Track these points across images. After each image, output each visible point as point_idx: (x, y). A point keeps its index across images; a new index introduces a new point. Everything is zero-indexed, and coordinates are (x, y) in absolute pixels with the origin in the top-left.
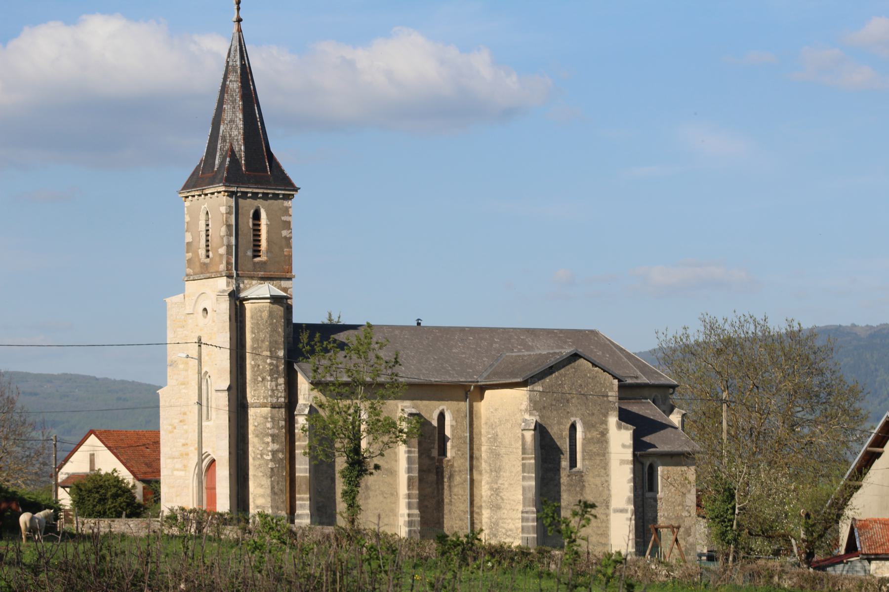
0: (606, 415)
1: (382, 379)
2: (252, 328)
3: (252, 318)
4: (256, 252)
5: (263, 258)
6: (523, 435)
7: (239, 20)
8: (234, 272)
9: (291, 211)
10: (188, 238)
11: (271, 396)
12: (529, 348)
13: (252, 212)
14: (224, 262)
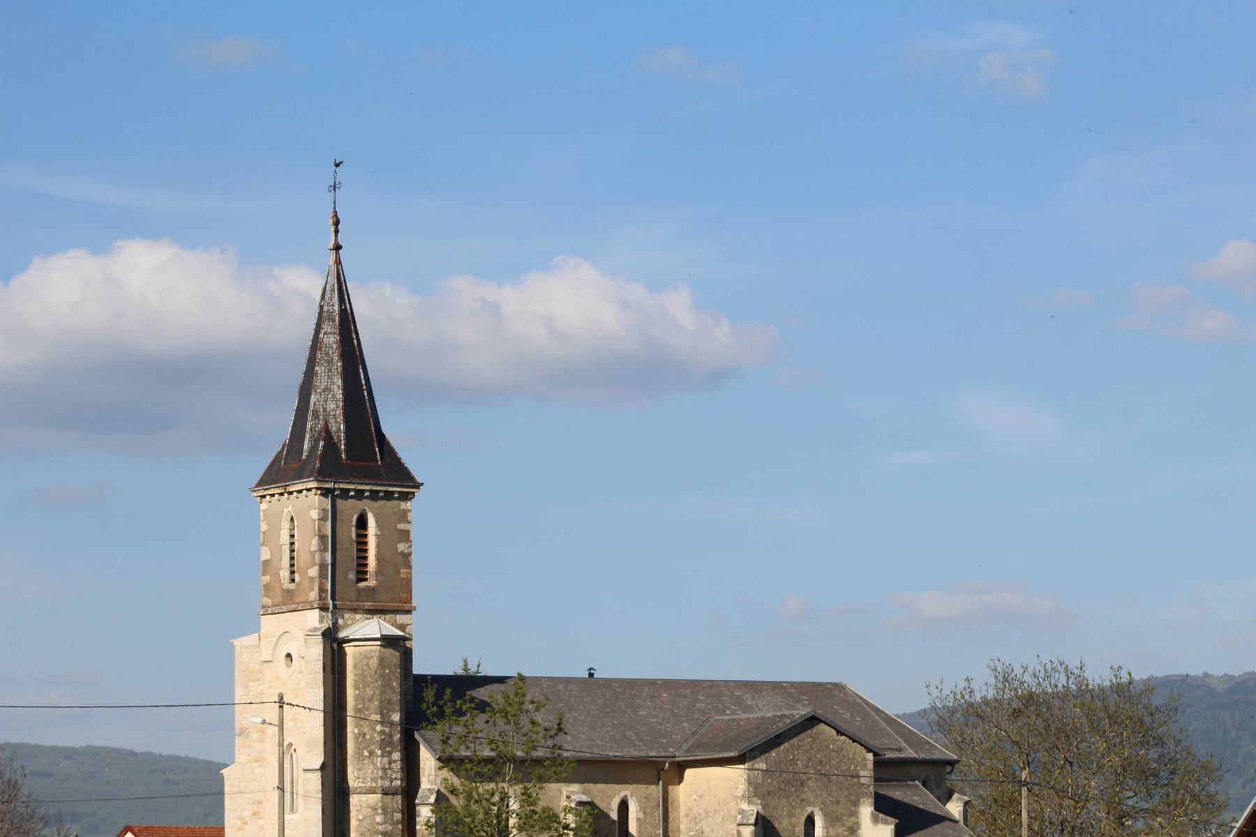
0: (856, 804)
1: (539, 753)
2: (356, 681)
3: (355, 667)
4: (362, 574)
5: (371, 582)
6: (739, 832)
7: (337, 248)
8: (330, 602)
9: (410, 516)
10: (265, 554)
11: (382, 778)
12: (747, 709)
13: (355, 517)
14: (316, 588)
